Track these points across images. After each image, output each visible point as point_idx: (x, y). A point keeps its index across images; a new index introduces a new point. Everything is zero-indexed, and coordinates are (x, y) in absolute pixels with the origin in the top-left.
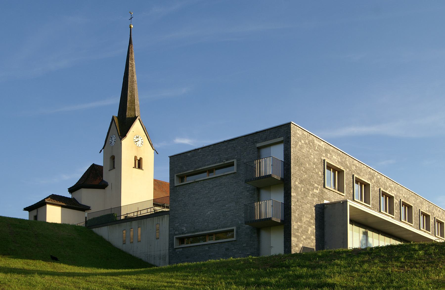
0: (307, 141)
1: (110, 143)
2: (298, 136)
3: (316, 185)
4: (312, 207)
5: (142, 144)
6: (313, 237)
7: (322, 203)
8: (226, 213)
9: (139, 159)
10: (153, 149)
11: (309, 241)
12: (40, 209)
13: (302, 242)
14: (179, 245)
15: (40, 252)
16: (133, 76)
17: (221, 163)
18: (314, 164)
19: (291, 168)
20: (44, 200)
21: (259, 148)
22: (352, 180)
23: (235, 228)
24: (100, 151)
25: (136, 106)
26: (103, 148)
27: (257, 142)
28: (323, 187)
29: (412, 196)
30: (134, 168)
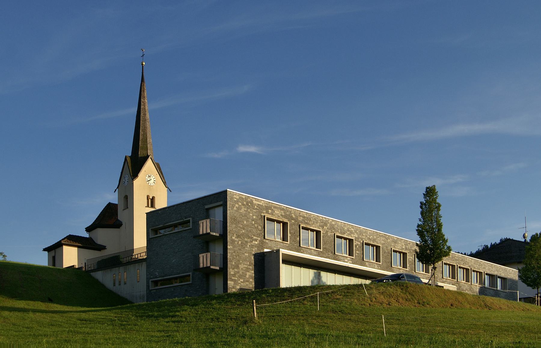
0: (245, 203)
1: (123, 182)
2: (236, 200)
3: (255, 238)
4: (250, 256)
5: (154, 183)
6: (252, 280)
7: (263, 251)
8: (186, 261)
9: (152, 198)
10: (166, 187)
11: (247, 283)
12: (58, 250)
13: (240, 285)
14: (155, 287)
15: (41, 295)
16: (145, 114)
17: (181, 221)
18: (253, 220)
19: (227, 226)
20: (60, 241)
21: (208, 210)
22: (299, 229)
23: (191, 273)
24: (115, 191)
25: (148, 145)
26: (118, 188)
27: (205, 204)
28: (263, 238)
29: (381, 237)
30: (146, 208)
